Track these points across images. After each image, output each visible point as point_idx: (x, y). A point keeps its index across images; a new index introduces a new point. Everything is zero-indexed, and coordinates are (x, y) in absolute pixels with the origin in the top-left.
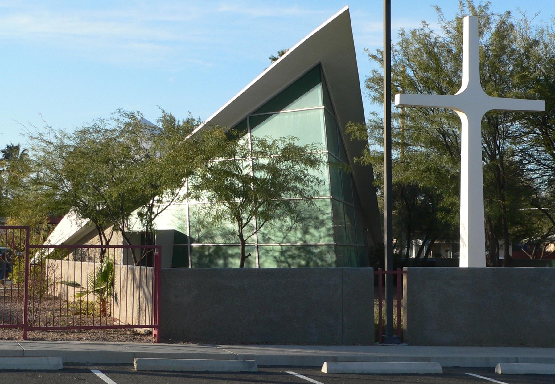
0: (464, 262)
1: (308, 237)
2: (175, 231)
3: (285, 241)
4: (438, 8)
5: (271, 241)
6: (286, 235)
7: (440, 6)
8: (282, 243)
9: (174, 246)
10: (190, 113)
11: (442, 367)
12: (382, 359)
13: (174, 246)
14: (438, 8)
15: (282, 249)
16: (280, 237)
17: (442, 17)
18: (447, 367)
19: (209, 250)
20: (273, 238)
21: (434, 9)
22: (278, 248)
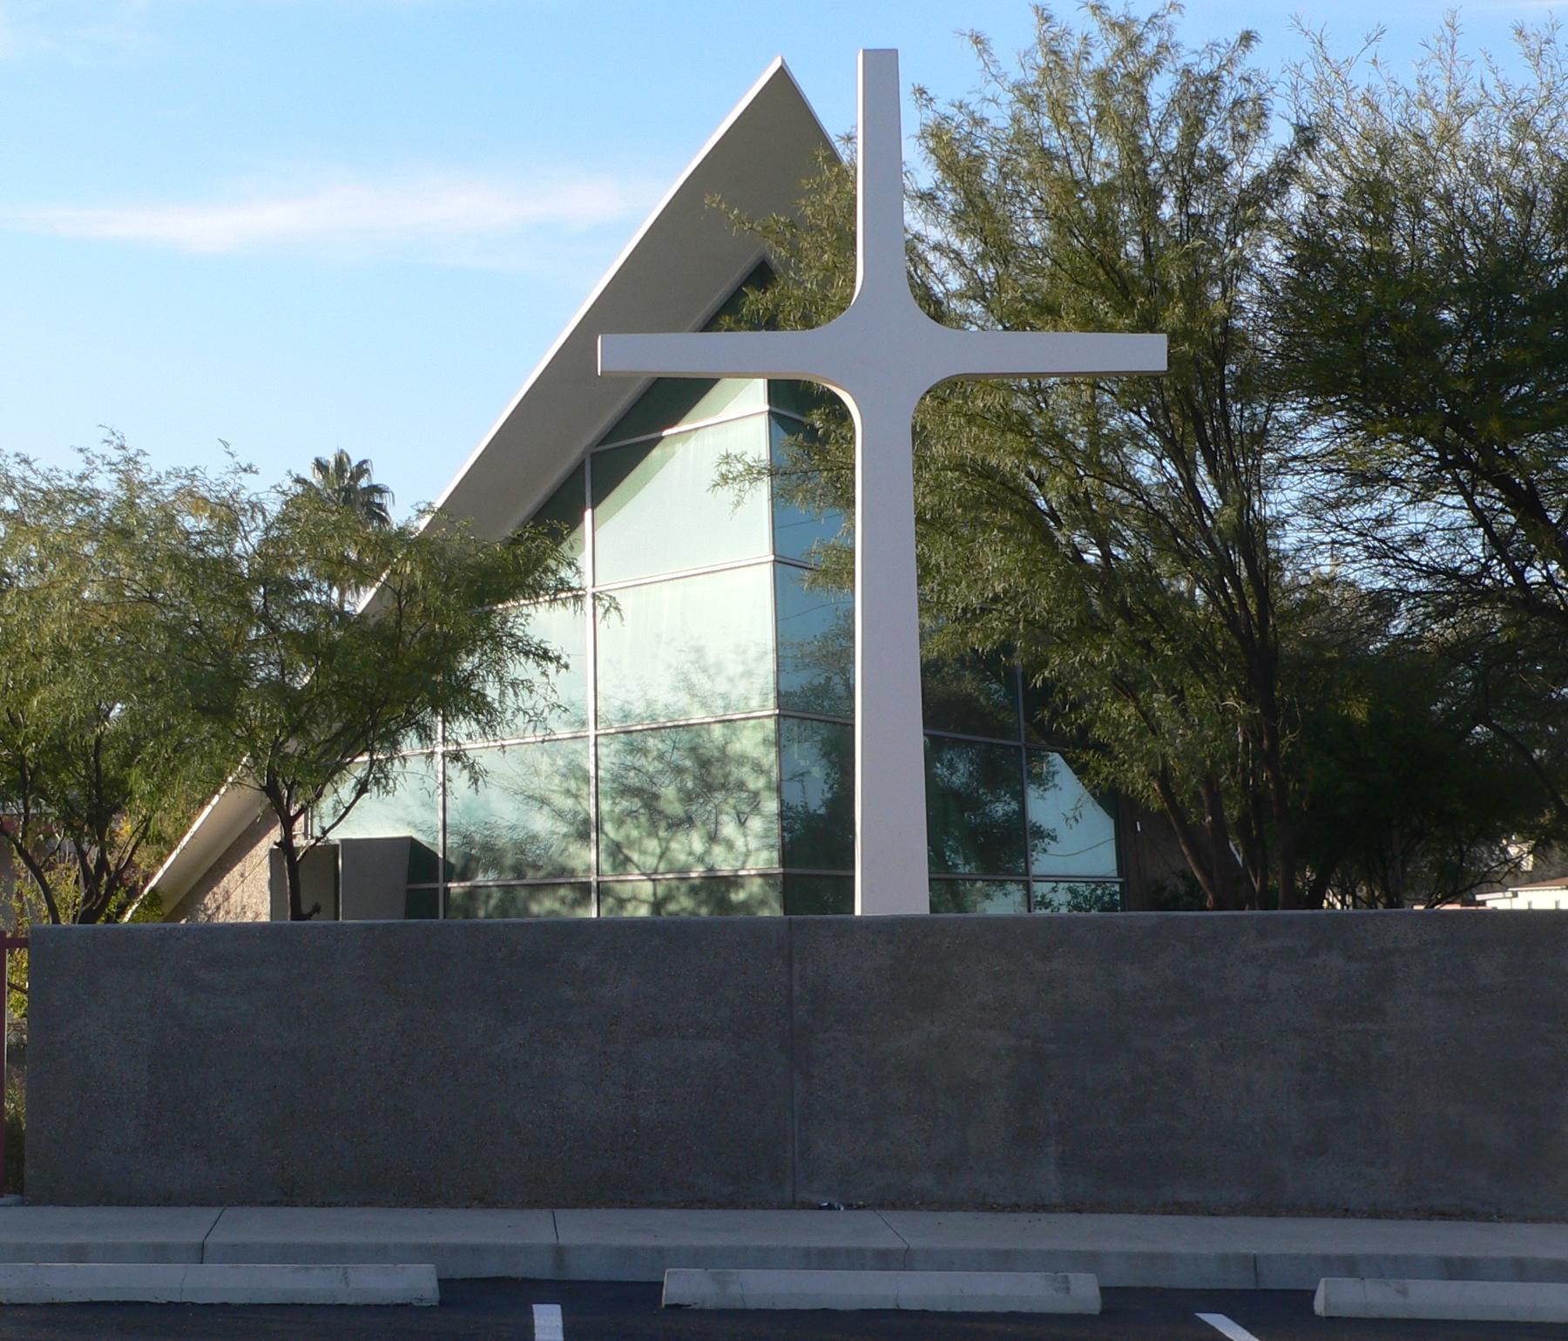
0: (858, 912)
1: (718, 851)
2: (412, 843)
3: (662, 867)
4: (977, 40)
5: (631, 868)
6: (667, 848)
7: (988, 32)
8: (656, 872)
9: (410, 891)
10: (226, 445)
11: (1102, 1289)
12: (826, 1259)
13: (410, 891)
14: (977, 40)
15: (655, 894)
16: (653, 854)
17: (994, 71)
18: (452, 1280)
19: (487, 902)
20: (635, 857)
21: (967, 41)
22: (646, 889)
